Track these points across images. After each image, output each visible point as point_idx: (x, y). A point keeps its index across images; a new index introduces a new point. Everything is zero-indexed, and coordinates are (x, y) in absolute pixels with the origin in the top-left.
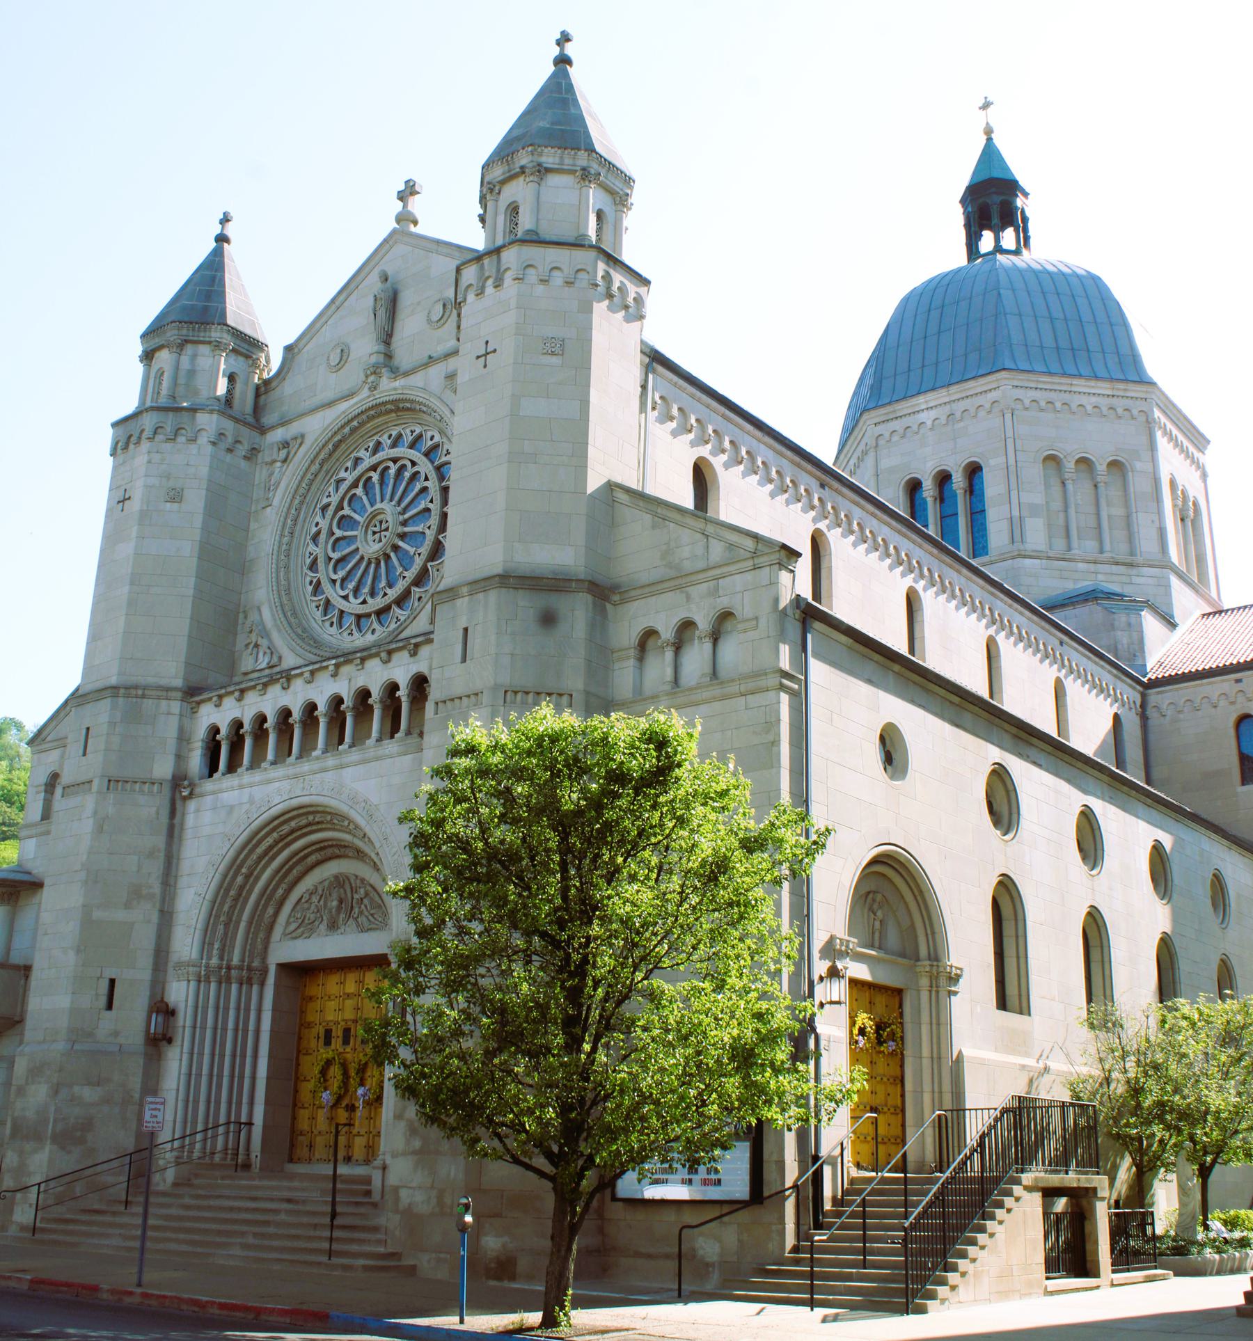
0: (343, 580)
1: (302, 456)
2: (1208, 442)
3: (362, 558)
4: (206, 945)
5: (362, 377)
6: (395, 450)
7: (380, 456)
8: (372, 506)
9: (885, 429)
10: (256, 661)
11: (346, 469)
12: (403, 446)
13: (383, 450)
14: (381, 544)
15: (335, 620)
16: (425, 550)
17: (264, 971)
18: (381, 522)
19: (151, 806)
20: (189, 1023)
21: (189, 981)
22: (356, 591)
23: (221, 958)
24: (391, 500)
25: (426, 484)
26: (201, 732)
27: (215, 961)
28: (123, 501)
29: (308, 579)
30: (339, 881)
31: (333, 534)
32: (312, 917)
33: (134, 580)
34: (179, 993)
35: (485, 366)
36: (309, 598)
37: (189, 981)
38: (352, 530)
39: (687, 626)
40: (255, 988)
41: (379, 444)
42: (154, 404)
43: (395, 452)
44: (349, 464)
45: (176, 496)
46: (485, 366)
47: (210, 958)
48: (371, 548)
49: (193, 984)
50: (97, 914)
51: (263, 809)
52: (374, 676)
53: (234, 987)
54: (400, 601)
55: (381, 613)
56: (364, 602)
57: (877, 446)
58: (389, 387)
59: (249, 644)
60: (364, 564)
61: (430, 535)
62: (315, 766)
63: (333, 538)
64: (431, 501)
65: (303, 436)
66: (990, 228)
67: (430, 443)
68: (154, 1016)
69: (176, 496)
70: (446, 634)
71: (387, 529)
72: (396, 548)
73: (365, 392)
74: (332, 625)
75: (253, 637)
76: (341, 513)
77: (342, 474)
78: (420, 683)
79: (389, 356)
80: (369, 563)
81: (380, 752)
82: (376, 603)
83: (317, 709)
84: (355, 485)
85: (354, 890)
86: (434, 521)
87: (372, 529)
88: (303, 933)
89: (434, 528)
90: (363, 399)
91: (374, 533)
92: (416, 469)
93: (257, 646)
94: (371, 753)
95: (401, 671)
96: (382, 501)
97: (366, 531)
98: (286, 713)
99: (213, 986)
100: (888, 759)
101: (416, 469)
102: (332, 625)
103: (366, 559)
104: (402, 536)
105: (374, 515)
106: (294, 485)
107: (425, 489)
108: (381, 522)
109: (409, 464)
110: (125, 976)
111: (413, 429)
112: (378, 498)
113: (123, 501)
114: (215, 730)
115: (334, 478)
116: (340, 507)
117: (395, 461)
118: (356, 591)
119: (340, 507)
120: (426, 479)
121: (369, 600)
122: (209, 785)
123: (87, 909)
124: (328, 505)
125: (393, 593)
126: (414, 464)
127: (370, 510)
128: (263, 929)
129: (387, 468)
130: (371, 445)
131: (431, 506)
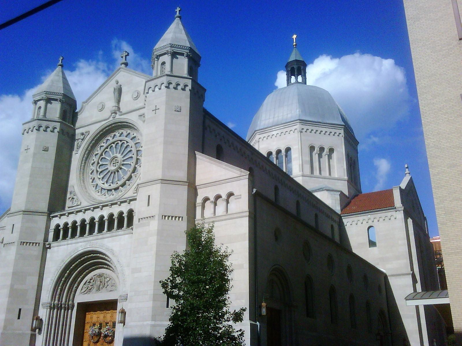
0: (103, 178)
1: (88, 139)
2: (205, 90)
3: (109, 171)
4: (53, 297)
5: (110, 114)
6: (120, 138)
7: (115, 139)
8: (113, 155)
9: (262, 136)
10: (73, 203)
11: (104, 143)
12: (129, 138)
13: (116, 137)
14: (116, 167)
15: (100, 191)
16: (131, 169)
17: (73, 306)
18: (116, 160)
19: (37, 251)
20: (47, 323)
21: (47, 309)
22: (107, 182)
23: (59, 301)
24: (122, 154)
25: (131, 149)
26: (53, 226)
27: (56, 302)
28: (28, 149)
29: (90, 177)
30: (100, 276)
31: (99, 163)
32: (91, 287)
33: (31, 176)
34: (43, 313)
35: (155, 113)
36: (91, 183)
37: (47, 309)
38: (106, 162)
39: (218, 197)
40: (70, 311)
41: (115, 135)
42: (38, 118)
43: (121, 138)
44: (105, 141)
45: (46, 150)
46: (155, 113)
47: (55, 301)
48: (112, 168)
49: (48, 310)
50: (16, 287)
51: (75, 252)
52: (115, 210)
53: (63, 310)
54: (123, 185)
55: (116, 189)
56: (110, 185)
57: (259, 142)
58: (119, 118)
59: (70, 198)
60: (109, 174)
61: (133, 165)
62: (95, 238)
63: (99, 165)
64: (133, 154)
65: (89, 131)
66: (294, 76)
67: (133, 136)
68: (35, 321)
69: (46, 150)
70: (142, 196)
71: (118, 163)
72: (121, 168)
73: (111, 119)
74: (98, 192)
75: (72, 195)
76: (102, 157)
77: (102, 144)
78: (131, 213)
79: (119, 108)
80: (112, 173)
81: (117, 234)
82: (114, 186)
83: (114, 216)
84: (107, 148)
85: (105, 278)
86: (134, 160)
87: (113, 162)
88: (87, 292)
89: (134, 163)
90: (111, 120)
91: (114, 164)
92: (128, 144)
93: (73, 198)
94: (114, 234)
95: (125, 208)
96: (119, 153)
97: (111, 162)
98: (102, 217)
99: (55, 310)
100: (276, 239)
101: (128, 144)
102: (98, 192)
103: (111, 172)
104: (123, 165)
105: (114, 158)
106: (86, 147)
107: (130, 151)
108: (116, 160)
109: (125, 142)
110: (24, 308)
111: (127, 131)
112: (115, 153)
113: (28, 149)
114: (58, 226)
115: (100, 145)
116: (102, 155)
117: (121, 141)
118: (107, 182)
119: (102, 155)
120: (131, 147)
121: (112, 185)
122: (54, 244)
123: (12, 286)
124: (98, 154)
125: (120, 183)
126: (127, 142)
127: (112, 156)
128: (72, 291)
129: (118, 143)
130: (113, 135)
131: (133, 156)
